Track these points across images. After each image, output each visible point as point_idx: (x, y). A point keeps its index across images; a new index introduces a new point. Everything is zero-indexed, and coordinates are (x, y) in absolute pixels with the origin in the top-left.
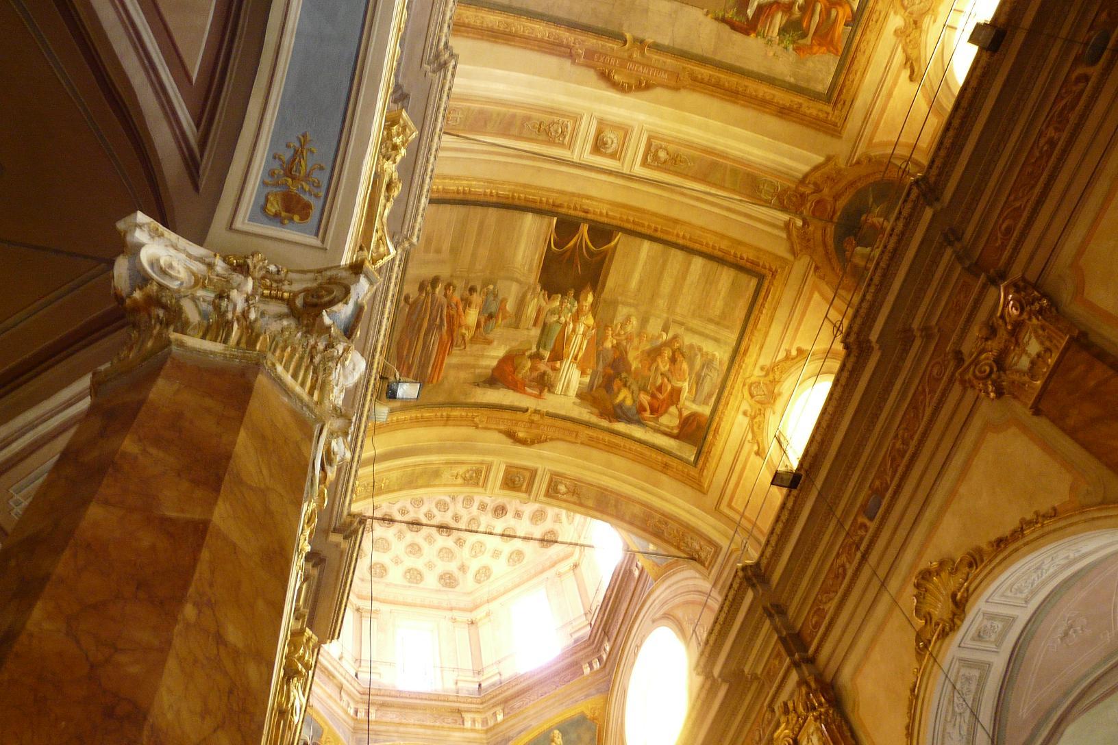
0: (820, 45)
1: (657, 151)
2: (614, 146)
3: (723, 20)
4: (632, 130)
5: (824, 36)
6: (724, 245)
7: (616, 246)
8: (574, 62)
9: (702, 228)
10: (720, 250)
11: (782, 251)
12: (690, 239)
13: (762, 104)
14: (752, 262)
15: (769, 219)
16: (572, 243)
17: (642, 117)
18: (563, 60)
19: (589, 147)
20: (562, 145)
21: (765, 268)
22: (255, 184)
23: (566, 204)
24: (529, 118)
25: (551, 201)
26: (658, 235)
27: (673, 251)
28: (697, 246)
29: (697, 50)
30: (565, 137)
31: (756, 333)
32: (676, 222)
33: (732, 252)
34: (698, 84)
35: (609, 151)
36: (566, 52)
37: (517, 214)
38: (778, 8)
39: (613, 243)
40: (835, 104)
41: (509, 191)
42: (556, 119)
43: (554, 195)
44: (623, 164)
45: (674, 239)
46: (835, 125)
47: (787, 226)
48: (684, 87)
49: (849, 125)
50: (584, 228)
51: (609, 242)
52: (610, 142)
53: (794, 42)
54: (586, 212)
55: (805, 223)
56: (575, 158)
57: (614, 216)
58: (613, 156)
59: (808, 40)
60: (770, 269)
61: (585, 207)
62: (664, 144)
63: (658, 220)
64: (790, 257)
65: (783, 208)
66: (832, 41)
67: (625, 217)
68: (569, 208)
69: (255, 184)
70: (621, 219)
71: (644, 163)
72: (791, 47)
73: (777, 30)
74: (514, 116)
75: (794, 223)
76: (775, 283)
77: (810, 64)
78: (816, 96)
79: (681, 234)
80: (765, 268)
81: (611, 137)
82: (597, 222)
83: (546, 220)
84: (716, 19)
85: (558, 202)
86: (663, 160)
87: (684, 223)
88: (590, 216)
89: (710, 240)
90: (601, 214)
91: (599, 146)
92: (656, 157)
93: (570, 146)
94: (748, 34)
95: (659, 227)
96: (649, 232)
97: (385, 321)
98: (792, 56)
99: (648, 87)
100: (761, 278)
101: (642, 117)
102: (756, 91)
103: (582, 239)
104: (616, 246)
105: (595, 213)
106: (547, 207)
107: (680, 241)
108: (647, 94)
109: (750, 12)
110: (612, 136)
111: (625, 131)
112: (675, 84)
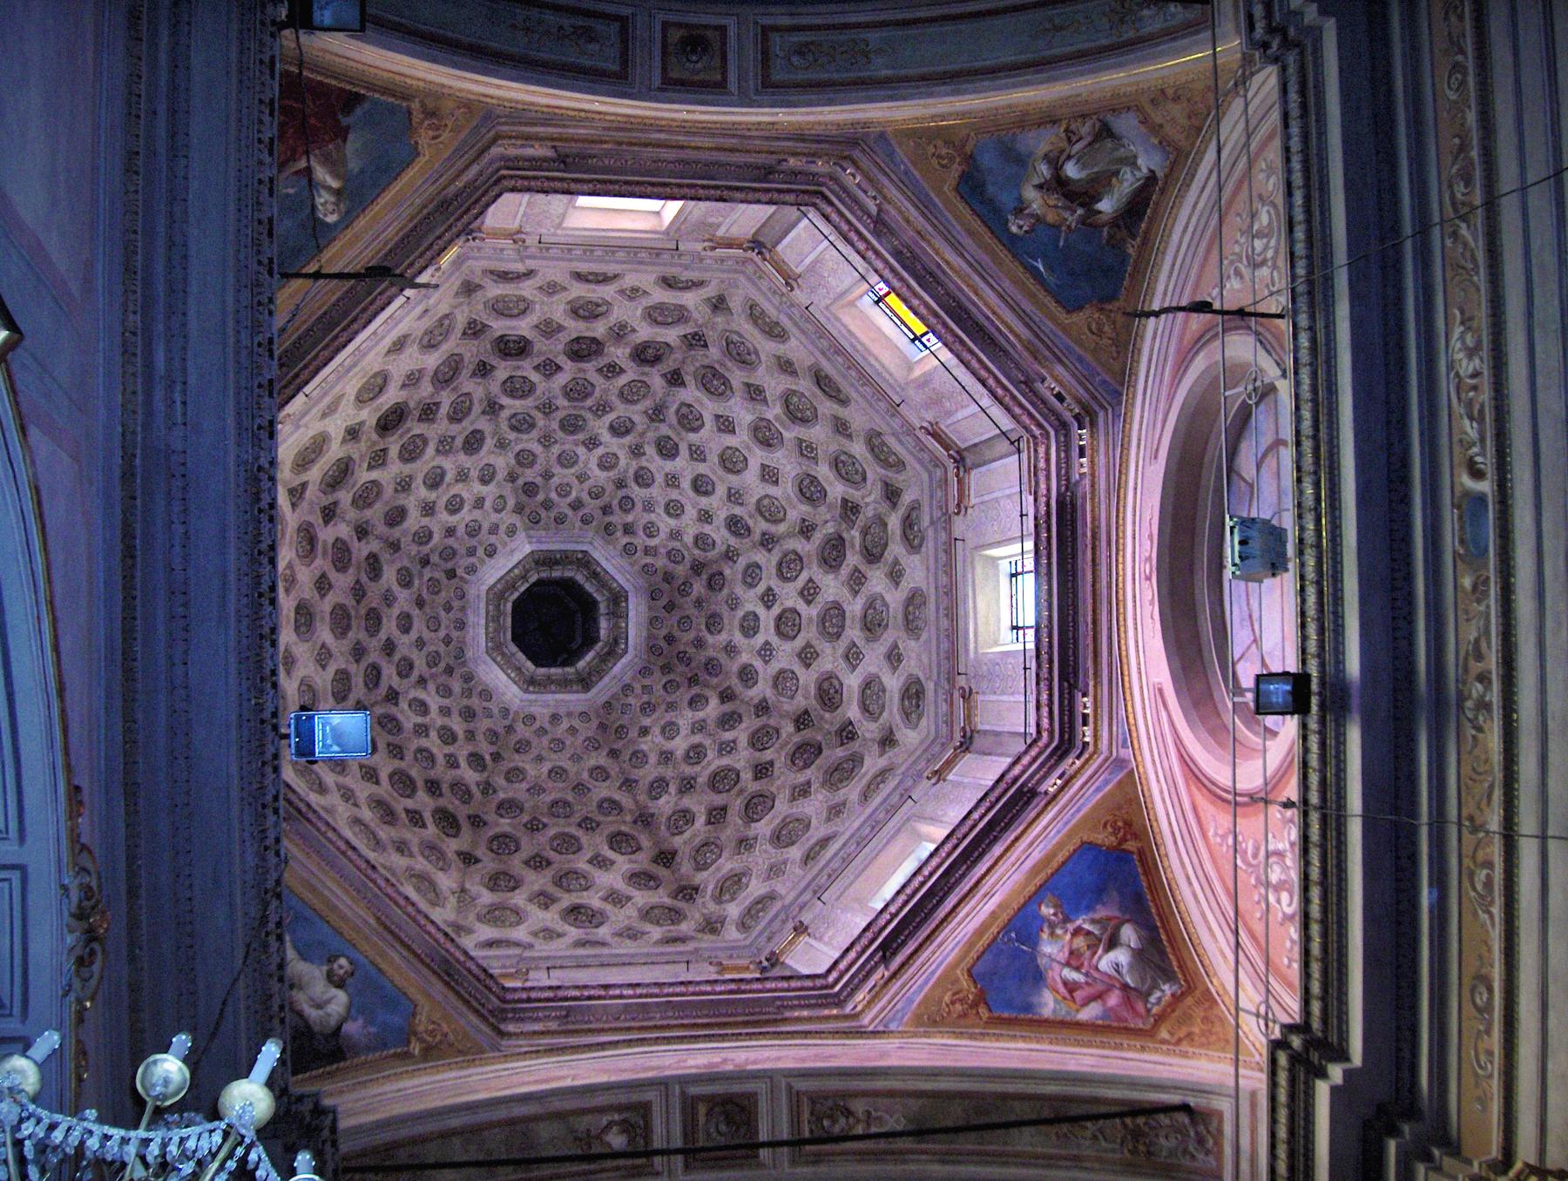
99: (130, 170)
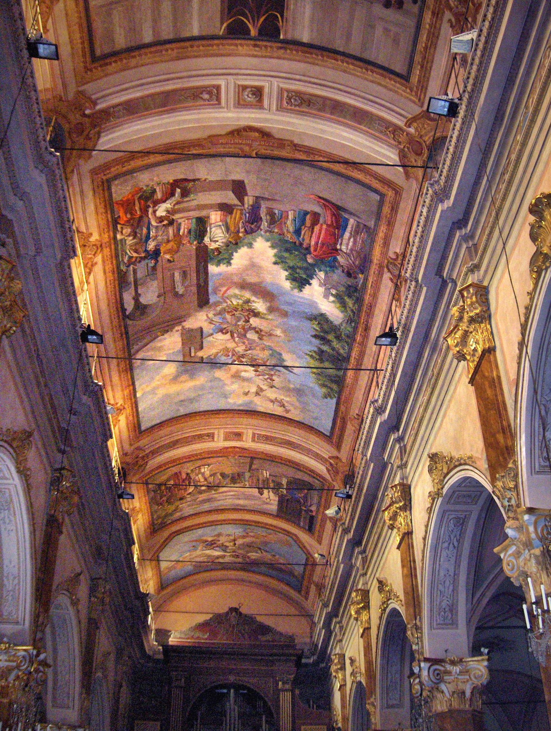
0: (129, 200)
1: (211, 97)
2: (246, 93)
3: (194, 180)
4: (234, 104)
5: (128, 205)
6: (133, 62)
7: (222, 24)
8: (292, 142)
9: (156, 63)
10: (134, 57)
11: (89, 88)
12: (161, 51)
13: (147, 153)
14: (106, 64)
15: (107, 98)
16: (262, 19)
17: (230, 115)
18: (299, 143)
19: (266, 90)
20: (288, 91)
21: (95, 67)
22: (538, 299)
23: (275, 49)
24: (319, 110)
25: (288, 51)
26: (188, 44)
27: (171, 37)
28: (153, 49)
29: (204, 161)
30: (287, 96)
31: (77, 20)
32: (179, 58)
33: (124, 61)
34: (197, 143)
35: (249, 89)
36: (296, 147)
37: (317, 42)
38: (162, 199)
39: (225, 25)
40: (103, 182)
41: (327, 61)
42: (297, 108)
43: (287, 56)
44: (235, 83)
45: (174, 45)
46: (97, 174)
47: (95, 103)
48: (205, 139)
49: (89, 181)
50: (253, 32)
51: (228, 26)
52: (250, 96)
53: (145, 191)
54: (255, 46)
55: (84, 115)
56: (275, 82)
57: (229, 46)
58: (245, 88)
59: (136, 198)
60: (91, 70)
61: (257, 49)
62: (207, 103)
63: (192, 54)
64: (80, 89)
65: (102, 111)
66: (122, 206)
67: (221, 47)
68: (271, 47)
69: (538, 299)
70: (223, 45)
71: (218, 88)
72: (145, 188)
73: (158, 190)
74: (332, 113)
75: (91, 109)
76: (82, 65)
77: (129, 188)
78: (116, 177)
79: (170, 51)
80: (95, 67)
81: (251, 99)
82: (244, 39)
83: (289, 37)
84: (198, 180)
85: (282, 51)
86: (204, 93)
87: (172, 60)
88: (252, 42)
89: (146, 59)
90: (241, 45)
91: (258, 92)
92: (210, 93)
93: (281, 91)
94: (175, 181)
95: (189, 49)
96: (197, 43)
97: (451, 149)
98: (142, 185)
99: (232, 133)
100: (94, 59)
101: (230, 115)
102: (155, 157)
103: (254, 21)
104: (222, 24)
105: (248, 45)
106: (291, 46)
107: (168, 46)
108: (229, 129)
109: (178, 190)
110: (249, 99)
111: (240, 104)
112: (213, 139)
